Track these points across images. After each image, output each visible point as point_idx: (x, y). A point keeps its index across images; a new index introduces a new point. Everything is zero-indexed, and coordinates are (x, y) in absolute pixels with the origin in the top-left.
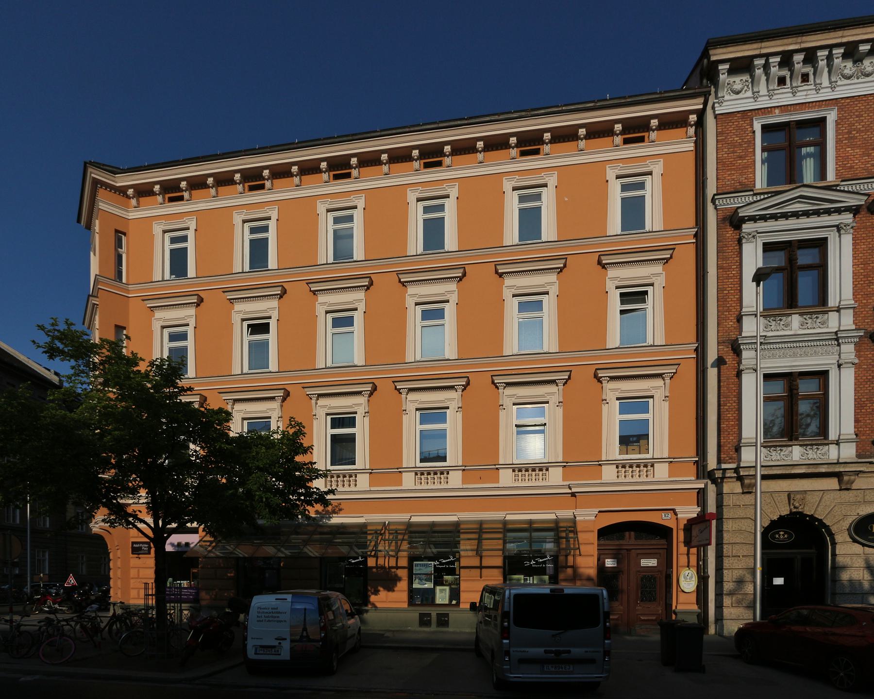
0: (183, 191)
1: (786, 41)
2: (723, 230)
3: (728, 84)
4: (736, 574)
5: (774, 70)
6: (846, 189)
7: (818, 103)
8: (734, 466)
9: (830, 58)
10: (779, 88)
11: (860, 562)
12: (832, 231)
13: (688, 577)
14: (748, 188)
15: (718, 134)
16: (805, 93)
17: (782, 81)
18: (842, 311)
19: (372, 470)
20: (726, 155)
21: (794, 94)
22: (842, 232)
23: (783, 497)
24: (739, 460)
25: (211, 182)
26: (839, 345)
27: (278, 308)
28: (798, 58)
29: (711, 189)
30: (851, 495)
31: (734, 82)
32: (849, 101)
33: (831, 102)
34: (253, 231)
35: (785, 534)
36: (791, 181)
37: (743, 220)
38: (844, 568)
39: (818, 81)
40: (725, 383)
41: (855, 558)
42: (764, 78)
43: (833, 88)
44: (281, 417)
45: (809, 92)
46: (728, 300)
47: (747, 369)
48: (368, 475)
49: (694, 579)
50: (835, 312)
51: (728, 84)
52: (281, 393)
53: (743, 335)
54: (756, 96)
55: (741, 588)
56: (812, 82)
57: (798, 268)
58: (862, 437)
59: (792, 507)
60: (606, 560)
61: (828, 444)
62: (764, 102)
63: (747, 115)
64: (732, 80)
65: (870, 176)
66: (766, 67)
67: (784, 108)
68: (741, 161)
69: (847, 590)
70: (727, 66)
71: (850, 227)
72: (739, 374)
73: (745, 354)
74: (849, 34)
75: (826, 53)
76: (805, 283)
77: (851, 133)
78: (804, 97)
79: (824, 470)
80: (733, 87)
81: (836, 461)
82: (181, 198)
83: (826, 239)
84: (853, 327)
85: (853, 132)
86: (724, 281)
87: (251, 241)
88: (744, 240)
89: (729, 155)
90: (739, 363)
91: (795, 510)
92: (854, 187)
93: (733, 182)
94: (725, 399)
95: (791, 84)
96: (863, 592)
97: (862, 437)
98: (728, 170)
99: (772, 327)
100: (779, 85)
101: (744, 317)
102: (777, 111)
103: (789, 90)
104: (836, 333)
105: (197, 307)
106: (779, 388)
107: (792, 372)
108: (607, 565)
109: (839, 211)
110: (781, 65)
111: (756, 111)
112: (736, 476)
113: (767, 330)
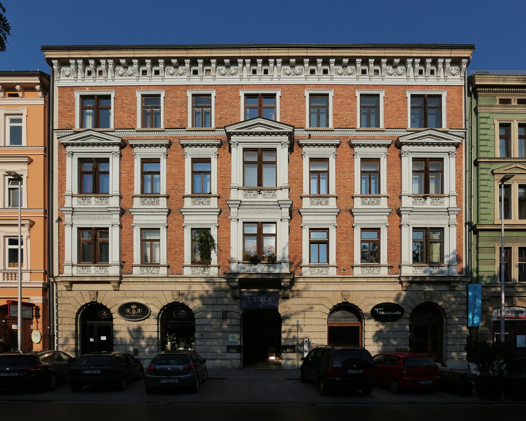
0: (18, 91)
1: (81, 52)
2: (61, 149)
3: (335, 69)
4: (65, 334)
5: (417, 66)
7: (107, 87)
8: (398, 276)
9: (444, 63)
10: (362, 75)
11: (125, 329)
13: (36, 335)
15: (60, 97)
16: (99, 81)
17: (421, 72)
18: (450, 197)
19: (31, 271)
20: (62, 109)
22: (450, 156)
23: (87, 293)
24: (401, 273)
25: (38, 88)
26: (449, 215)
28: (429, 61)
29: (56, 126)
30: (119, 293)
31: (452, 69)
32: (122, 88)
33: (113, 87)
34: (12, 121)
35: (106, 313)
36: (426, 127)
37: (402, 144)
38: (118, 331)
39: (438, 75)
40: (61, 231)
41: (122, 326)
42: (412, 69)
43: (446, 80)
44: (30, 237)
45: (102, 81)
46: (63, 187)
47: (452, 224)
48: (29, 273)
49: (39, 336)
51: (335, 69)
52: (28, 222)
53: (402, 206)
54: (408, 78)
55: (139, 342)
56: (436, 75)
57: (92, 173)
58: (127, 263)
59: (344, 299)
60: (13, 325)
62: (80, 83)
63: (72, 88)
64: (388, 68)
65: (132, 128)
66: (413, 63)
68: (69, 113)
69: (119, 344)
70: (386, 60)
71: (454, 153)
72: (400, 227)
73: (403, 216)
74: (335, 52)
75: (411, 60)
77: (123, 105)
78: (100, 83)
79: (99, 280)
80: (389, 72)
82: (17, 95)
83: (443, 158)
84: (456, 206)
85: (124, 104)
86: (61, 176)
87: (11, 127)
88: (403, 155)
89: (64, 109)
90: (401, 221)
91: (345, 301)
92: (457, 133)
93: (65, 124)
94: (61, 240)
95: (437, 74)
96: (126, 344)
97: (127, 263)
98: (63, 117)
101: (402, 196)
102: (87, 88)
103: (436, 77)
104: (447, 209)
105: (28, 165)
106: (420, 236)
107: (427, 227)
108: (13, 328)
109: (449, 145)
110: (363, 63)
111: (78, 87)
112: (399, 281)
113: (414, 204)
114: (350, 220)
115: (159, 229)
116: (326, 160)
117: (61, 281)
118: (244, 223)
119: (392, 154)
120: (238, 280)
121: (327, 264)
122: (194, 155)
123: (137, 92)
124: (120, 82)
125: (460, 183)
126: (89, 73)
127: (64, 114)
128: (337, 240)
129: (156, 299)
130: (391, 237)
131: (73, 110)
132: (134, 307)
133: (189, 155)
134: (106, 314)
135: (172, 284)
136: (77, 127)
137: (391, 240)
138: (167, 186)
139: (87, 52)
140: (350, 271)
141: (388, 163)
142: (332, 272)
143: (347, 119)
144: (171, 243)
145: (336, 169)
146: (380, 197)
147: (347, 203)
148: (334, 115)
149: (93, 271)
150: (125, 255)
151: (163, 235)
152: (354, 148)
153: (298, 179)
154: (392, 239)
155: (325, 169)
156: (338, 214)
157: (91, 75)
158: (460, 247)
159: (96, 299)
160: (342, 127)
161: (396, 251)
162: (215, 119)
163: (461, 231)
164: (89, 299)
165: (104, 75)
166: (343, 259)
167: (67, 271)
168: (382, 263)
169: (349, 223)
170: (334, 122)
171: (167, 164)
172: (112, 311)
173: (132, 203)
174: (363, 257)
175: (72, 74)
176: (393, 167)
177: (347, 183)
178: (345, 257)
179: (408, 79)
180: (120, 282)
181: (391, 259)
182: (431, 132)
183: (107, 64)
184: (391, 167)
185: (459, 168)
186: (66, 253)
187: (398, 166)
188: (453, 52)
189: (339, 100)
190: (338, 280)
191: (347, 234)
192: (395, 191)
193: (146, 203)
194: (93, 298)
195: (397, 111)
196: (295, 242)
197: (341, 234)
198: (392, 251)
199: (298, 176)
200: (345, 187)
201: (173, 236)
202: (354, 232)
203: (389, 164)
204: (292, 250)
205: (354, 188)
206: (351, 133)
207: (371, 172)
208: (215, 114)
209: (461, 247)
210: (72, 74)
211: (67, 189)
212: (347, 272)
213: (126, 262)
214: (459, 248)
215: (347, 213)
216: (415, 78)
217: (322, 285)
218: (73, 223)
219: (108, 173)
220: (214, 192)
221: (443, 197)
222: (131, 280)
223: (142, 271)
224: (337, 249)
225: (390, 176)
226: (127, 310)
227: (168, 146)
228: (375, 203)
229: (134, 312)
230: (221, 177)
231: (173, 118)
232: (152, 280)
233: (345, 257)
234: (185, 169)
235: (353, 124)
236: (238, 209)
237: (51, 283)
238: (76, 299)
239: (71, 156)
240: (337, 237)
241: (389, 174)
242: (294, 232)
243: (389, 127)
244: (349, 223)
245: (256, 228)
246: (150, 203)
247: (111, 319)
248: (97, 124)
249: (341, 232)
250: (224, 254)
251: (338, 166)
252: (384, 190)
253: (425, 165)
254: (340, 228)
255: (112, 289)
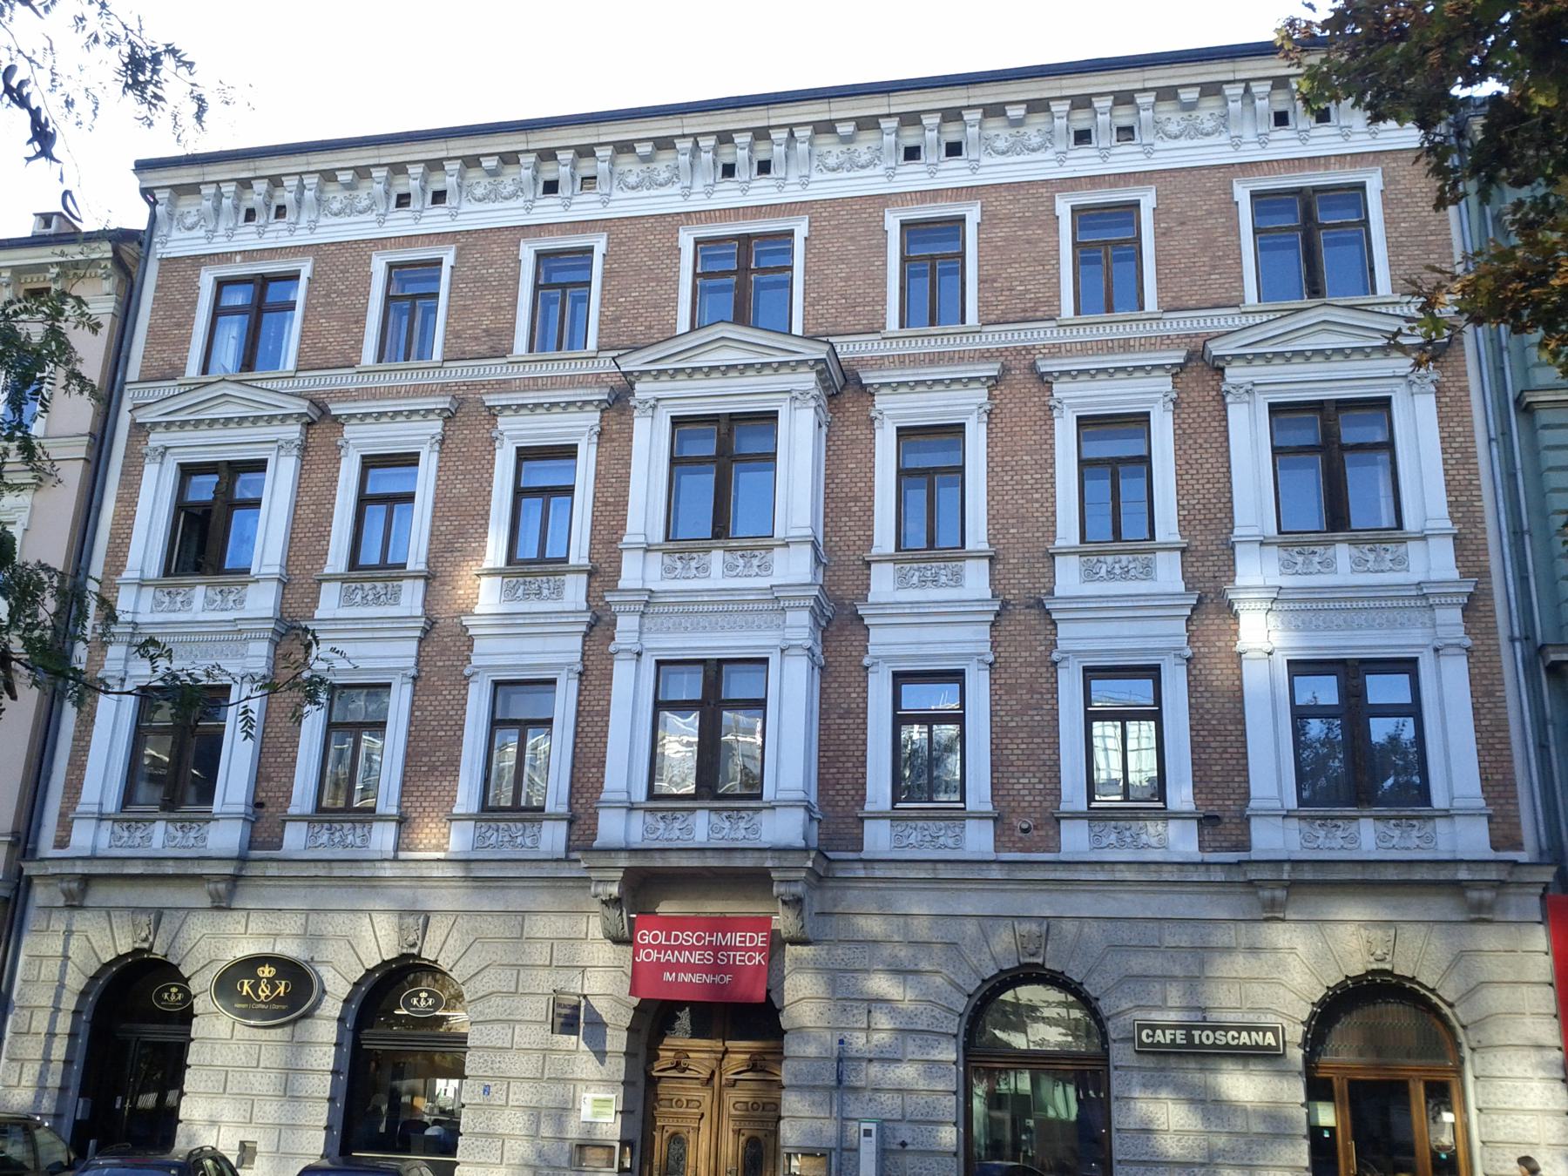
6: (1384, 310)
12: (1397, 385)
14: (1236, 303)
15: (158, 288)
16: (274, 234)
21: (566, 207)
27: (28, 510)
29: (133, 373)
45: (281, 233)
47: (1447, 645)
50: (1275, 548)
61: (1431, 818)
67: (249, 255)
76: (1362, 480)
81: (87, 853)
88: (1229, 399)
99: (1297, 568)
100: (1277, 124)
102: (238, 258)
114: (1042, 637)
115: (553, 682)
116: (1139, 421)
117: (55, 875)
118: (659, 663)
119: (1192, 394)
120: (621, 874)
121: (1160, 805)
122: (1083, 405)
123: (374, 256)
124: (827, 186)
125: (1471, 484)
126: (250, 215)
127: (171, 334)
128: (993, 714)
129: (342, 943)
130: (1203, 700)
131: (189, 320)
132: (266, 974)
133: (510, 438)
134: (176, 994)
135: (406, 887)
136: (193, 369)
137: (1208, 712)
138: (431, 542)
139: (252, 165)
140: (1047, 836)
141: (1180, 428)
142: (979, 839)
143: (1027, 291)
144: (423, 734)
145: (990, 459)
146: (1153, 551)
147: (1031, 575)
148: (981, 281)
149: (160, 837)
150: (269, 779)
151: (398, 706)
152: (1222, 369)
153: (856, 499)
154: (1208, 706)
155: (1380, 437)
156: (1192, 611)
157: (284, 215)
158: (1497, 734)
159: (151, 938)
160: (1011, 317)
161: (1228, 756)
162: (601, 322)
163: (1495, 671)
164: (130, 941)
165: (290, 216)
166: (1020, 786)
167: (83, 837)
168: (971, 804)
169: (1039, 649)
170: (983, 303)
171: (440, 469)
172: (194, 987)
173: (316, 601)
174: (899, 788)
175: (202, 223)
176: (1199, 441)
177: (1029, 505)
178: (1026, 781)
179: (1236, 146)
180: (235, 879)
181: (1211, 785)
182: (1325, 314)
183: (219, 196)
184: (1191, 442)
185: (1460, 429)
186: (88, 773)
187: (1216, 435)
188: (771, 112)
189: (1000, 233)
190: (996, 873)
191: (1032, 691)
192: (1213, 527)
193: (358, 598)
194: (143, 935)
195: (1204, 249)
196: (841, 721)
197: (1011, 689)
198: (1215, 756)
199: (856, 489)
200: (1022, 520)
201: (430, 708)
202: (1057, 682)
203: (1184, 430)
204: (831, 754)
205: (1054, 523)
206: (1039, 334)
207: (936, 470)
208: (602, 305)
209: (1501, 734)
210: (202, 223)
211: (129, 564)
212: (1037, 839)
213: (268, 804)
214: (1493, 737)
215: (1033, 611)
216: (1263, 140)
217: (938, 894)
218: (126, 673)
219: (256, 504)
220: (416, 560)
221: (1403, 541)
222: (273, 870)
223: (315, 836)
224: (996, 749)
225: (1191, 472)
226: (242, 985)
227: (994, 383)
228: (1133, 572)
229: (264, 992)
230: (606, 504)
231: (471, 328)
232: (338, 871)
233: (1026, 781)
234: (494, 484)
235: (1048, 303)
236: (643, 614)
237: (23, 879)
238: (88, 940)
239: (159, 459)
240: (993, 704)
241: (1188, 467)
242: (840, 687)
243: (1176, 304)
244: (1039, 649)
245: (701, 675)
246: (369, 598)
247: (187, 1016)
248: (248, 362)
249: (1009, 681)
250: (594, 770)
251: (996, 449)
252: (1168, 527)
253: (1324, 426)
254: (1006, 669)
255: (207, 903)
